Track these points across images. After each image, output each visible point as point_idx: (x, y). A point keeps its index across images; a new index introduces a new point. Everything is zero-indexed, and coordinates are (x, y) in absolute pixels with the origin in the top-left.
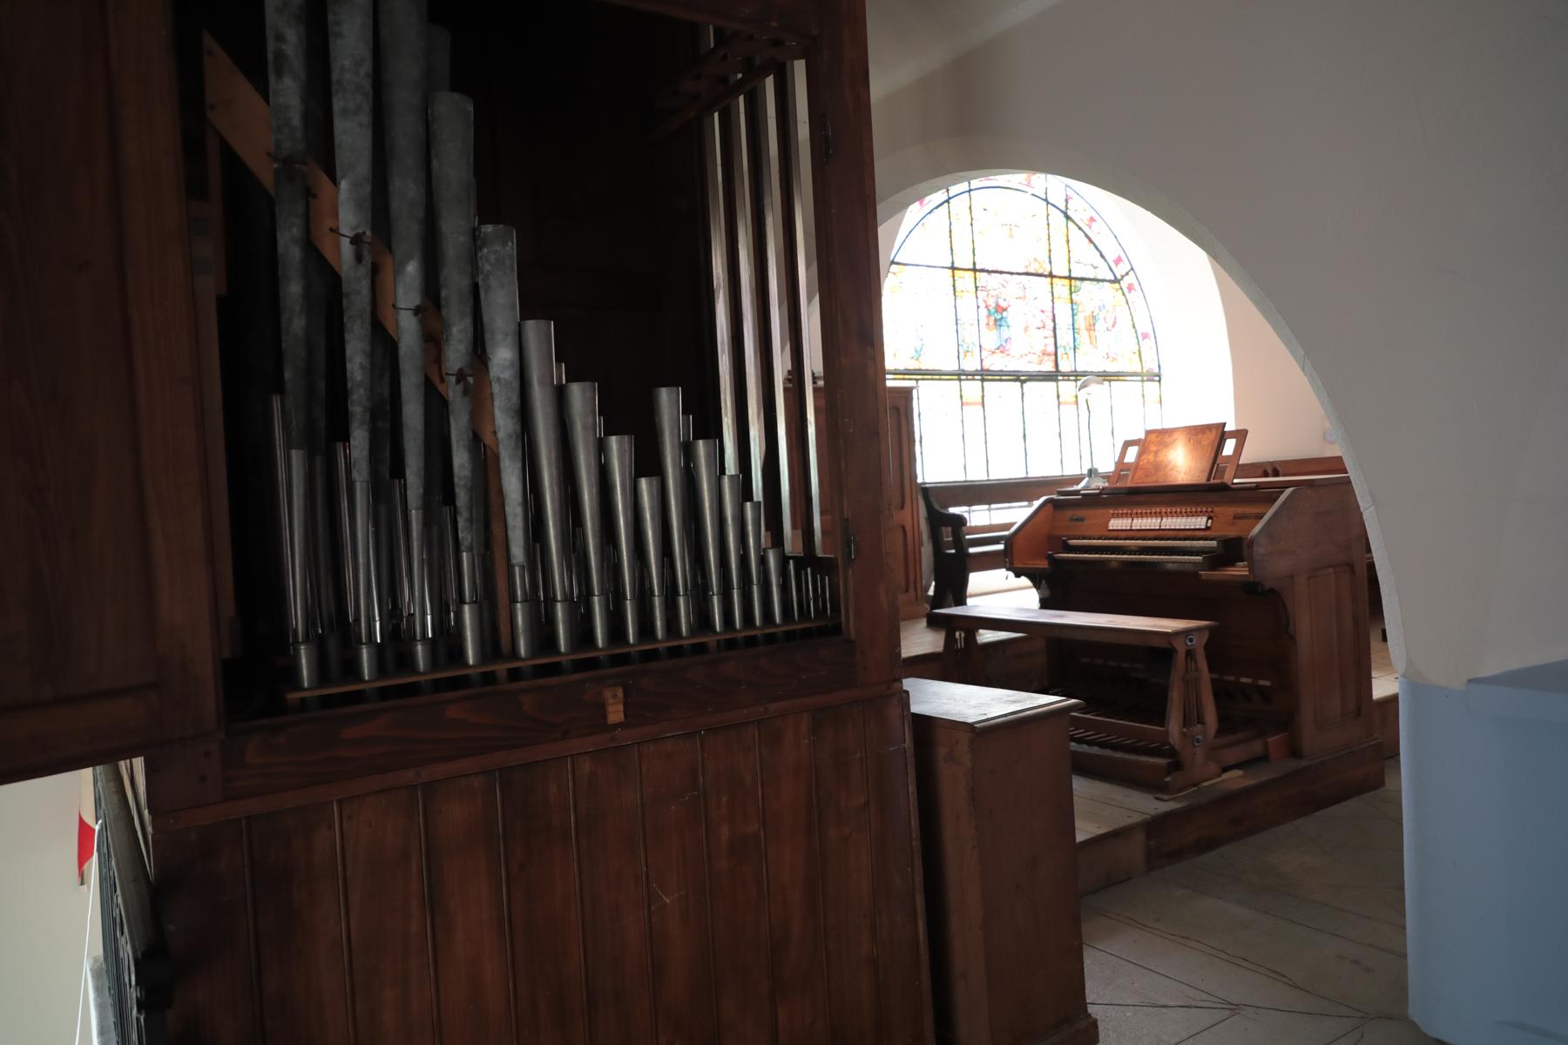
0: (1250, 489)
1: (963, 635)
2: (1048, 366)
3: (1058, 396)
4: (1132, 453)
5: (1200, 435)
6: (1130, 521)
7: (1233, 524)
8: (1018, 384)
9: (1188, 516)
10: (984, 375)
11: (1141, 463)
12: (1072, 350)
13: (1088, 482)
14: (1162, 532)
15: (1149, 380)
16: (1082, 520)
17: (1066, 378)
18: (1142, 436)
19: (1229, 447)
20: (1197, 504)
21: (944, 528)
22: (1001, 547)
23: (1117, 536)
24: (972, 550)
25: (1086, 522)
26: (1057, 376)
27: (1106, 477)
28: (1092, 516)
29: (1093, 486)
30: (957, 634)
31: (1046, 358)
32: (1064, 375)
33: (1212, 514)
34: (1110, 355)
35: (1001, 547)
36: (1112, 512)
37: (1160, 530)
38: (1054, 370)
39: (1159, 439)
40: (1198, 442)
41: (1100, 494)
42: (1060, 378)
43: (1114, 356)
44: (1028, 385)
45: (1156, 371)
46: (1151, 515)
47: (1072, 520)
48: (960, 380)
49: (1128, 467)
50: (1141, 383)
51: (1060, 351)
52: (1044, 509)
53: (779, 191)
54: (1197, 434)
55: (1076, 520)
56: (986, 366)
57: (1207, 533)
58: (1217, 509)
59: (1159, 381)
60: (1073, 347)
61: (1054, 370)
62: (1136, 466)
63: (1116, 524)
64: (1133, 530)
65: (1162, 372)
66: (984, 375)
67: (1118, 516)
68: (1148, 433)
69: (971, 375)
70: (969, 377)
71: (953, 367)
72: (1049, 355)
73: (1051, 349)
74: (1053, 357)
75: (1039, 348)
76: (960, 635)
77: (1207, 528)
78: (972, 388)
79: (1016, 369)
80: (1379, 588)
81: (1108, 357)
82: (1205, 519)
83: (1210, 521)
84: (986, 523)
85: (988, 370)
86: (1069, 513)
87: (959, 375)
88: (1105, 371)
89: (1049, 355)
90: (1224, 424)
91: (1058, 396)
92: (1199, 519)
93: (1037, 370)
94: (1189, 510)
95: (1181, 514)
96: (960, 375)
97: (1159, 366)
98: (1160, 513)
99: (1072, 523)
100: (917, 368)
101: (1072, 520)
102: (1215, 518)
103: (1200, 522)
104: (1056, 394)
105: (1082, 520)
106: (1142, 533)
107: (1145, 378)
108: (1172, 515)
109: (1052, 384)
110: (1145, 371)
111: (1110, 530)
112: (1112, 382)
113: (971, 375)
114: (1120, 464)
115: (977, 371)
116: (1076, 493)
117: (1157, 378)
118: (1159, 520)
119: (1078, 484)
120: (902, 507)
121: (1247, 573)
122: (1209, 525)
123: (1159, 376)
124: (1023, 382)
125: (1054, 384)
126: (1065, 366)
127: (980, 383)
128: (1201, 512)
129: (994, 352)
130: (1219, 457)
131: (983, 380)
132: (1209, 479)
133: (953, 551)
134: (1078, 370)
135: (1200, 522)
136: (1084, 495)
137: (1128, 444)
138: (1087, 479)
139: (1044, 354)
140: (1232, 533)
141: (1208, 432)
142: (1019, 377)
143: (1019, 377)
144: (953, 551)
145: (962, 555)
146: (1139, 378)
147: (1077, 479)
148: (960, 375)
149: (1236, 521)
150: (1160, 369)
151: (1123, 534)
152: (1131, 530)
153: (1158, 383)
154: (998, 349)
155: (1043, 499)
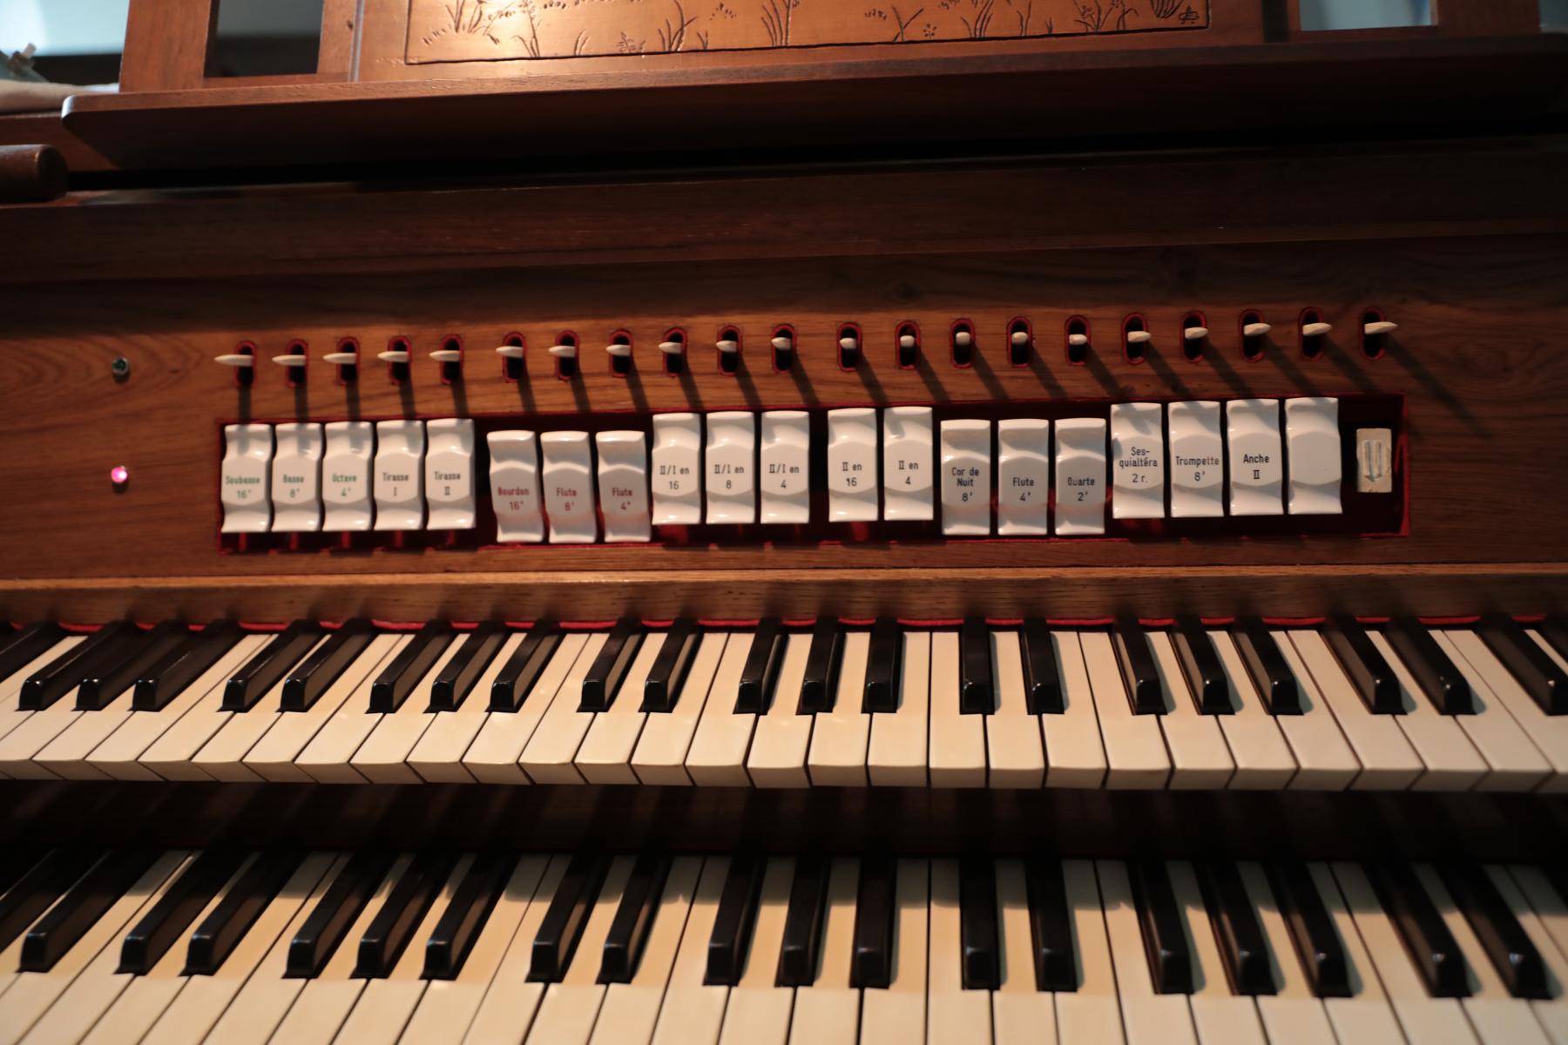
33: (1385, 374)
83: (1375, 446)
102: (1421, 412)
122: (1376, 474)
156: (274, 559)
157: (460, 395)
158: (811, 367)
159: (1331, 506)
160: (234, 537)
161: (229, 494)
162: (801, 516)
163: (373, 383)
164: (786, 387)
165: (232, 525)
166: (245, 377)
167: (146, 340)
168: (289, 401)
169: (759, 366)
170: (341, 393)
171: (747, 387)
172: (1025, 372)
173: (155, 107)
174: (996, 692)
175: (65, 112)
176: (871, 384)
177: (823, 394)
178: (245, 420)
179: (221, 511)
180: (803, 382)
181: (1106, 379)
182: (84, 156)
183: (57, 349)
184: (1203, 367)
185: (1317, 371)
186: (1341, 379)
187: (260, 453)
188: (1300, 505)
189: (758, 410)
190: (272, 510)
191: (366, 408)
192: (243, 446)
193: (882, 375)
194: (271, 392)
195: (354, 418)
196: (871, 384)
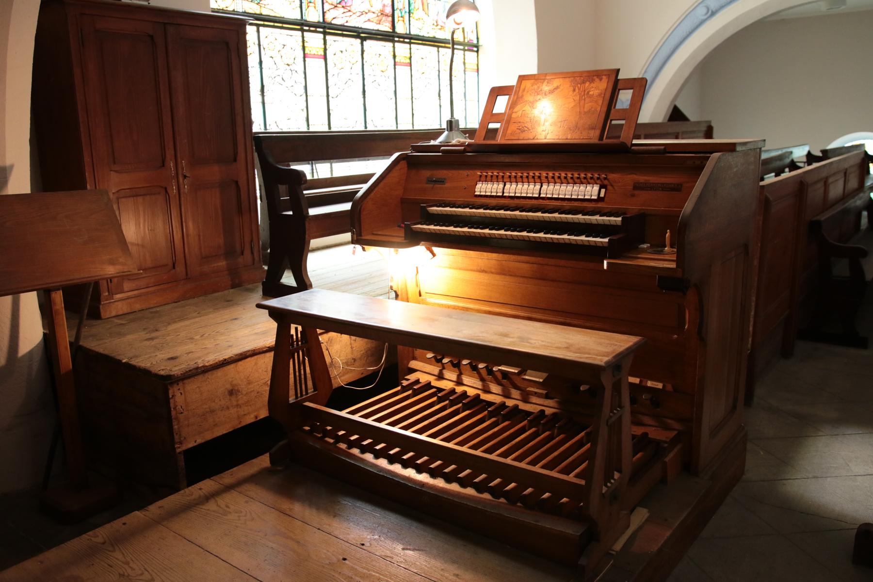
0: (657, 152)
1: (300, 328)
2: (386, 27)
3: (394, 56)
4: (501, 104)
5: (587, 84)
6: (501, 186)
7: (633, 196)
8: (359, 41)
9: (575, 183)
10: (326, 28)
11: (514, 115)
12: (408, 14)
13: (448, 136)
14: (541, 202)
15: (469, 50)
16: (441, 181)
17: (402, 40)
18: (512, 81)
19: (625, 97)
20: (586, 169)
21: (280, 187)
22: (347, 206)
23: (487, 202)
24: (313, 212)
25: (447, 185)
26: (393, 37)
27: (471, 133)
28: (456, 178)
29: (454, 142)
30: (293, 326)
31: (384, 18)
32: (400, 36)
33: (606, 182)
34: (439, 23)
35: (347, 206)
36: (479, 173)
37: (539, 198)
38: (391, 31)
39: (536, 87)
40: (584, 95)
41: (464, 151)
42: (396, 39)
43: (443, 25)
44: (367, 43)
45: (475, 42)
46: (528, 180)
47: (430, 181)
48: (303, 31)
49: (497, 118)
50: (462, 52)
51: (397, 13)
52: (397, 168)
53: (562, 478)
54: (584, 82)
55: (435, 181)
56: (329, 18)
57: (600, 205)
58: (612, 176)
59: (477, 51)
60: (408, 11)
61: (391, 31)
62: (506, 118)
63: (484, 188)
64: (505, 197)
65: (480, 43)
66: (326, 28)
67: (486, 179)
68: (522, 78)
69: (314, 27)
70: (312, 29)
71: (295, 15)
72: (387, 15)
73: (388, 10)
74: (390, 19)
75: (377, 7)
76: (296, 329)
77: (600, 199)
78: (314, 40)
79: (357, 26)
80: (34, 64)
81: (437, 25)
82: (596, 188)
83: (603, 191)
84: (294, 390)
85: (331, 24)
86: (426, 173)
87: (302, 25)
88: (434, 37)
89: (387, 15)
90: (618, 71)
91: (394, 56)
92: (589, 188)
93: (376, 28)
94: (576, 175)
95: (566, 181)
96: (302, 25)
97: (478, 38)
98: (539, 177)
99: (431, 186)
100: (258, 12)
101: (430, 181)
102: (609, 187)
103: (591, 191)
104: (392, 54)
105: (441, 181)
106: (517, 201)
107: (466, 48)
108: (555, 181)
109: (389, 45)
110: (466, 41)
111: (476, 196)
112: (440, 49)
113: (314, 27)
114: (489, 114)
115: (319, 22)
116: (435, 148)
117: (475, 49)
118: (538, 186)
119: (435, 139)
120: (235, 160)
121: (673, 265)
122: (602, 195)
123: (477, 46)
124: (363, 39)
125: (390, 44)
126: (400, 29)
127: (322, 36)
128: (591, 178)
129: (336, 7)
130: (613, 111)
131: (325, 34)
132: (601, 138)
133: (291, 213)
134: (412, 33)
135: (591, 191)
136: (444, 152)
137: (496, 92)
138: (446, 133)
139: (382, 14)
140: (634, 207)
141: (597, 80)
142: (361, 35)
143: (361, 35)
144: (291, 213)
145: (301, 216)
146: (462, 47)
147: (436, 134)
148: (302, 25)
149: (636, 192)
150: (478, 41)
151: (493, 202)
152: (503, 197)
153: (476, 53)
154: (340, 3)
155: (396, 155)
156: (480, 198)
157: (503, 180)
158: (542, 178)
159: (596, 198)
160: (476, 195)
161: (476, 190)
162: (537, 196)
163: (494, 177)
164: (539, 181)
165: (476, 193)
166: (481, 176)
167: (471, 171)
168: (484, 179)
169: (556, 178)
170: (490, 179)
171: (534, 180)
172: (565, 180)
173: (209, 436)
174: (357, 159)
175: (467, 144)
176: (548, 181)
177: (543, 181)
178: (480, 181)
179: (475, 192)
180: (541, 180)
181: (574, 181)
182: (468, 149)
183: (461, 172)
184: (585, 180)
185: (598, 182)
186: (600, 183)
187: (546, 187)
188: (593, 197)
189: (549, 183)
190: (486, 192)
191: (505, 181)
192: (479, 184)
193: (549, 179)
194: (483, 178)
195: (491, 182)
196: (548, 181)
